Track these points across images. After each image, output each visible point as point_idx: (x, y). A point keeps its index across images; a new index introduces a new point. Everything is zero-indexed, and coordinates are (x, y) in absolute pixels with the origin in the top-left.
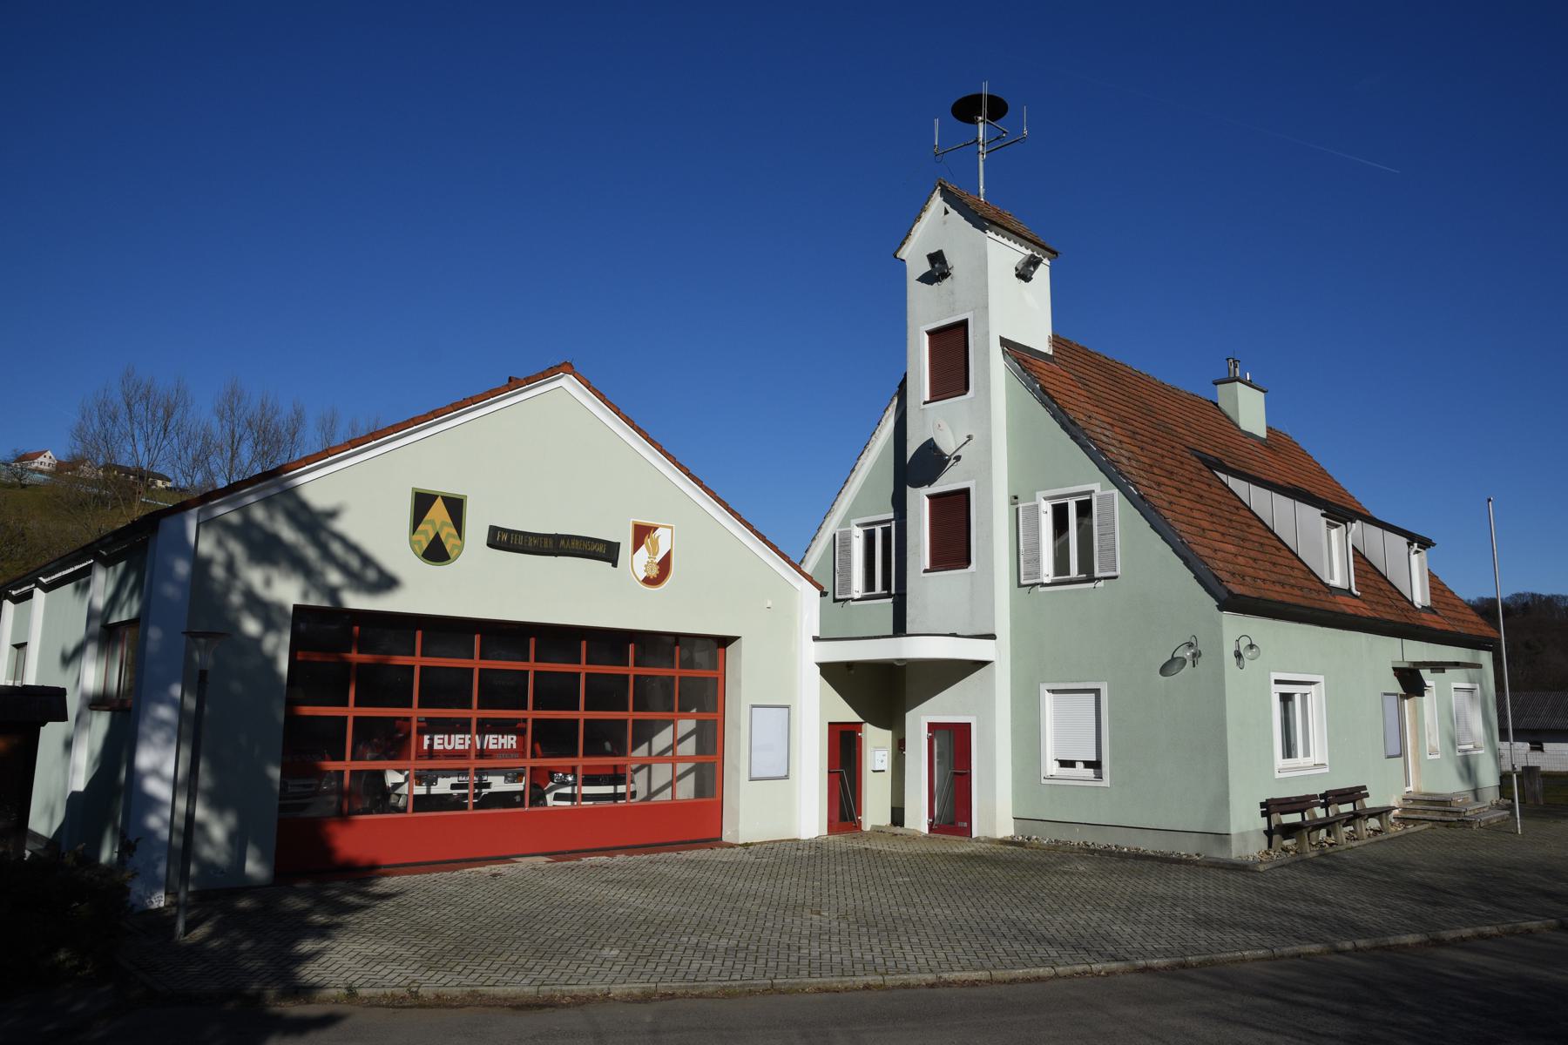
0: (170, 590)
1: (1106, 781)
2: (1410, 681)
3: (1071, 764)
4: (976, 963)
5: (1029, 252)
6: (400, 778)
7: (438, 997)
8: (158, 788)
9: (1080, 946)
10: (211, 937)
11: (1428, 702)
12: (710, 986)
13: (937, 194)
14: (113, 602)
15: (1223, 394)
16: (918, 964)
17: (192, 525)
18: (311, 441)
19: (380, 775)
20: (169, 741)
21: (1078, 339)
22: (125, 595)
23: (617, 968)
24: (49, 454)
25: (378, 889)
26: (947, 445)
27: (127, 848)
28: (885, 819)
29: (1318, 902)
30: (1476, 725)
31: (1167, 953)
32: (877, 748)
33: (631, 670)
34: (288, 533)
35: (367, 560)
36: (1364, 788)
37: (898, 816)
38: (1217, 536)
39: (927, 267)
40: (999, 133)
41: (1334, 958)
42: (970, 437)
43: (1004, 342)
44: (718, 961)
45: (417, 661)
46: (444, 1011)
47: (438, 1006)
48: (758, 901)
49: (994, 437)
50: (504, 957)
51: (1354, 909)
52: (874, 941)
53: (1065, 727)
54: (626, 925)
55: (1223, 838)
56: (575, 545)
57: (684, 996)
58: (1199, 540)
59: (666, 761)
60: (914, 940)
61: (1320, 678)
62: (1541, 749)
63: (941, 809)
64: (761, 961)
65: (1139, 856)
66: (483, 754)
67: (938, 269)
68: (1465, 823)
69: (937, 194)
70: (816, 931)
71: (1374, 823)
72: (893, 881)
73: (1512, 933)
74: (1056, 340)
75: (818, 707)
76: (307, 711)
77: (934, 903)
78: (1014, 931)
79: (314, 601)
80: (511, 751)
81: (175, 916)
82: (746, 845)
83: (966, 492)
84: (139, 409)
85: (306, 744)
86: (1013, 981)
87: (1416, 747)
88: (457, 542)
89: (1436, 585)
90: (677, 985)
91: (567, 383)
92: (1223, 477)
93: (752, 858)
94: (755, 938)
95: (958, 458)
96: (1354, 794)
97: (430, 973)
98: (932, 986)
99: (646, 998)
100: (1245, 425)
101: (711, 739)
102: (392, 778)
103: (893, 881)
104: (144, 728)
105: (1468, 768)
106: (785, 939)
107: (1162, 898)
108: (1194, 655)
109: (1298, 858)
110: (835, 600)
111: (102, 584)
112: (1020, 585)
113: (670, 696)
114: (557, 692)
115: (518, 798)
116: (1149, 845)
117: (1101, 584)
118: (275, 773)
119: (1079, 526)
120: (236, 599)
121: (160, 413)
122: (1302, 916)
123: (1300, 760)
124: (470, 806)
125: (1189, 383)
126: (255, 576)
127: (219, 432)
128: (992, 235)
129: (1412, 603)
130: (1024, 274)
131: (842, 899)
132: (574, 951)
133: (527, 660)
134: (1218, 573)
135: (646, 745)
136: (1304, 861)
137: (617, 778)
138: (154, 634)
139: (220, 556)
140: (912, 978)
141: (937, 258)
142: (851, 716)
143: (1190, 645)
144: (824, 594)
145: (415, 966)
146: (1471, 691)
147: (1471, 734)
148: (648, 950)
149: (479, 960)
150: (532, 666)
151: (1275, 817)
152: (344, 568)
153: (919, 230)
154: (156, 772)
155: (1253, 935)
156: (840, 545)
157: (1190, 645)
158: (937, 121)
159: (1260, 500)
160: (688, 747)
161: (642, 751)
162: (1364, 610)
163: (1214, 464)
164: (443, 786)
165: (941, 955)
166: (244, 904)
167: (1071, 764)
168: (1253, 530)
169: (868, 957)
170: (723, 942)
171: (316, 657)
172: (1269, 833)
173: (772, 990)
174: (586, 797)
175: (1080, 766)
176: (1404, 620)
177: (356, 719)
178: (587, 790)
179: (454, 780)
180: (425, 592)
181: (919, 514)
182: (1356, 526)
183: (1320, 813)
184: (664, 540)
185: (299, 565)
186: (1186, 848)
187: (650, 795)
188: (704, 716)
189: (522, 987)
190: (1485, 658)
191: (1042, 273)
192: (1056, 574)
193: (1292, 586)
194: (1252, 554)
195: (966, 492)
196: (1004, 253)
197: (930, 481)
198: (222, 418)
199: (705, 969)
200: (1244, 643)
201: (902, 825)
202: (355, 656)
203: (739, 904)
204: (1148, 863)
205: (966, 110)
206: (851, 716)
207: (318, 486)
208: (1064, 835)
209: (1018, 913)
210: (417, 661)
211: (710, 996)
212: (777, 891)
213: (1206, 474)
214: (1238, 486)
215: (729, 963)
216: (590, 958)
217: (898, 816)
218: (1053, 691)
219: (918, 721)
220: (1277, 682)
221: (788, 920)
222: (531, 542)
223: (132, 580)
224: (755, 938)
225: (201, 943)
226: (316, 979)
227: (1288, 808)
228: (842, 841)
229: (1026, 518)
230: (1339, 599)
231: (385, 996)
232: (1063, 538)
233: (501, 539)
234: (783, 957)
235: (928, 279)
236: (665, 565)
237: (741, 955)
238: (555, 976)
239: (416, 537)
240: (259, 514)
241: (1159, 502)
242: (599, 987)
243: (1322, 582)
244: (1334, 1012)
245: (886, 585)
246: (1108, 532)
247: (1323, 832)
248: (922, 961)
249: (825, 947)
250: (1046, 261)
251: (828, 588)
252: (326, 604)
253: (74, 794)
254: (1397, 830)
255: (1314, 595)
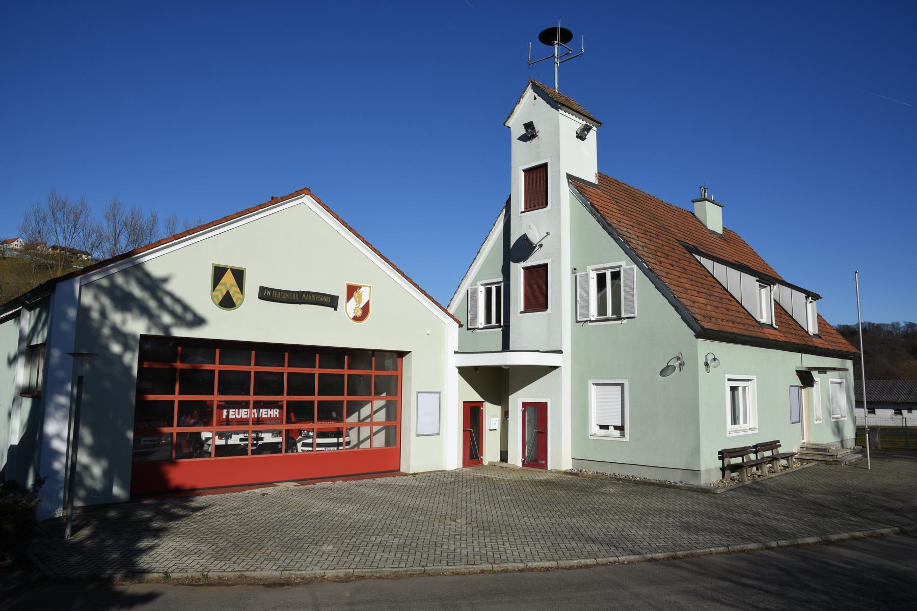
0: (65, 327)
1: (627, 438)
2: (806, 379)
3: (606, 427)
4: (549, 556)
5: (584, 123)
6: (210, 435)
7: (220, 578)
8: (60, 446)
9: (612, 544)
10: (89, 538)
11: (816, 390)
12: (387, 571)
13: (530, 87)
14: (34, 330)
15: (697, 208)
16: (514, 556)
17: (77, 287)
18: (161, 232)
19: (199, 434)
20: (65, 417)
21: (612, 175)
22: (40, 326)
23: (331, 558)
24: (20, 240)
25: (193, 504)
26: (534, 238)
27: (38, 482)
28: (497, 458)
29: (754, 514)
30: (843, 401)
31: (664, 549)
32: (492, 417)
33: (346, 371)
34: (137, 291)
35: (186, 308)
36: (778, 441)
37: (504, 457)
38: (695, 293)
39: (523, 132)
40: (567, 51)
41: (766, 552)
42: (548, 233)
43: (569, 177)
44: (392, 554)
45: (217, 367)
46: (222, 588)
47: (220, 584)
48: (419, 512)
49: (563, 234)
50: (263, 551)
51: (775, 519)
52: (488, 540)
53: (603, 406)
54: (339, 528)
55: (696, 473)
56: (312, 297)
57: (370, 578)
58: (684, 295)
59: (367, 424)
60: (512, 539)
61: (754, 377)
62: (874, 413)
63: (529, 453)
64: (419, 554)
65: (646, 483)
66: (258, 421)
67: (530, 132)
68: (837, 462)
69: (530, 87)
70: (452, 533)
71: (784, 462)
72: (500, 499)
73: (872, 536)
74: (600, 176)
75: (458, 392)
76: (151, 397)
77: (524, 514)
78: (572, 534)
79: (154, 332)
80: (276, 418)
81: (65, 525)
82: (414, 474)
83: (545, 266)
84: (59, 215)
85: (149, 417)
86: (571, 568)
87: (808, 417)
88: (241, 296)
89: (821, 322)
90: (366, 571)
91: (307, 200)
92: (698, 257)
93: (417, 483)
94: (416, 538)
95: (541, 246)
96: (773, 445)
97: (216, 562)
98: (521, 571)
99: (347, 579)
100: (710, 227)
101: (394, 411)
102: (205, 435)
103: (500, 499)
104: (50, 409)
105: (838, 428)
106: (434, 539)
107: (660, 511)
108: (680, 364)
109: (740, 485)
110: (468, 329)
111: (27, 320)
112: (577, 322)
113: (369, 386)
114: (301, 385)
115: (280, 446)
116: (652, 476)
117: (625, 321)
118: (130, 435)
119: (612, 285)
120: (106, 331)
121: (72, 217)
122: (745, 524)
123: (741, 425)
124: (249, 453)
125: (678, 201)
126: (116, 317)
127: (107, 230)
128: (562, 112)
129: (807, 332)
130: (581, 136)
131: (469, 511)
132: (305, 547)
133: (283, 366)
134: (696, 316)
135: (357, 413)
136: (744, 487)
137: (338, 434)
138: (56, 353)
139: (96, 306)
140: (510, 566)
141: (529, 126)
142: (476, 397)
143: (678, 359)
144: (461, 326)
145: (208, 557)
146: (840, 383)
147: (840, 408)
148: (351, 546)
149: (247, 553)
150: (286, 370)
151: (726, 460)
152: (172, 313)
153: (519, 109)
154: (58, 436)
155: (716, 536)
156: (471, 296)
157: (678, 359)
158: (530, 44)
159: (720, 271)
160: (381, 416)
161: (353, 419)
162: (781, 337)
163: (692, 250)
164: (235, 440)
165: (527, 550)
166: (112, 514)
167: (606, 427)
168: (716, 289)
169: (483, 551)
170: (397, 540)
171: (157, 366)
172: (723, 469)
173: (425, 573)
174: (319, 445)
175: (611, 428)
176: (803, 343)
177: (180, 402)
178: (319, 441)
179: (242, 436)
180: (221, 326)
181: (517, 279)
182: (776, 287)
183: (753, 457)
184: (365, 295)
185: (145, 311)
186: (674, 478)
187: (360, 442)
188: (390, 398)
189: (271, 572)
190: (849, 364)
191: (592, 135)
192: (599, 314)
193: (739, 323)
194: (716, 304)
195: (546, 266)
196: (570, 123)
197: (524, 259)
198: (109, 220)
199: (384, 559)
200: (710, 357)
201: (506, 462)
202: (179, 365)
203: (408, 514)
204: (651, 487)
205: (548, 37)
206: (476, 397)
207: (156, 263)
208: (602, 469)
209: (574, 520)
210: (217, 367)
211: (386, 578)
212: (431, 505)
213: (688, 256)
214: (707, 263)
215: (399, 555)
216: (314, 551)
217: (504, 457)
218: (596, 384)
219: (517, 400)
220: (729, 380)
221: (436, 525)
222: (285, 296)
223: (44, 317)
224: (416, 538)
225: (80, 542)
226: (147, 566)
227: (734, 454)
228: (471, 472)
229: (581, 281)
230: (766, 330)
231: (187, 578)
232: (603, 292)
233: (267, 294)
234: (432, 551)
235: (524, 138)
236: (366, 309)
237: (407, 549)
238: (293, 564)
239: (215, 293)
240: (120, 280)
241: (660, 273)
242: (318, 572)
243: (756, 320)
244: (768, 592)
245: (498, 321)
246: (630, 290)
247: (754, 468)
248: (516, 554)
249: (458, 544)
250: (594, 128)
251: (464, 322)
252: (161, 334)
253: (12, 447)
254: (797, 466)
255: (751, 328)
